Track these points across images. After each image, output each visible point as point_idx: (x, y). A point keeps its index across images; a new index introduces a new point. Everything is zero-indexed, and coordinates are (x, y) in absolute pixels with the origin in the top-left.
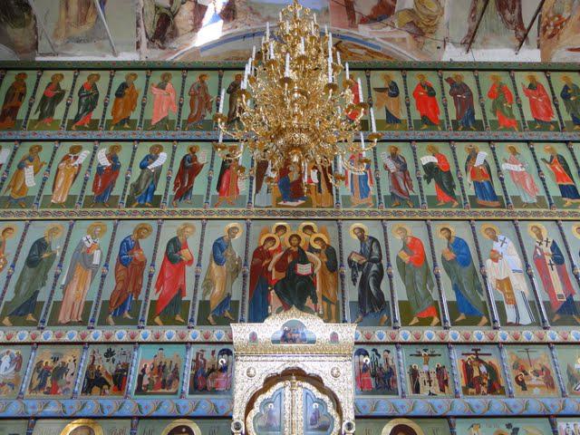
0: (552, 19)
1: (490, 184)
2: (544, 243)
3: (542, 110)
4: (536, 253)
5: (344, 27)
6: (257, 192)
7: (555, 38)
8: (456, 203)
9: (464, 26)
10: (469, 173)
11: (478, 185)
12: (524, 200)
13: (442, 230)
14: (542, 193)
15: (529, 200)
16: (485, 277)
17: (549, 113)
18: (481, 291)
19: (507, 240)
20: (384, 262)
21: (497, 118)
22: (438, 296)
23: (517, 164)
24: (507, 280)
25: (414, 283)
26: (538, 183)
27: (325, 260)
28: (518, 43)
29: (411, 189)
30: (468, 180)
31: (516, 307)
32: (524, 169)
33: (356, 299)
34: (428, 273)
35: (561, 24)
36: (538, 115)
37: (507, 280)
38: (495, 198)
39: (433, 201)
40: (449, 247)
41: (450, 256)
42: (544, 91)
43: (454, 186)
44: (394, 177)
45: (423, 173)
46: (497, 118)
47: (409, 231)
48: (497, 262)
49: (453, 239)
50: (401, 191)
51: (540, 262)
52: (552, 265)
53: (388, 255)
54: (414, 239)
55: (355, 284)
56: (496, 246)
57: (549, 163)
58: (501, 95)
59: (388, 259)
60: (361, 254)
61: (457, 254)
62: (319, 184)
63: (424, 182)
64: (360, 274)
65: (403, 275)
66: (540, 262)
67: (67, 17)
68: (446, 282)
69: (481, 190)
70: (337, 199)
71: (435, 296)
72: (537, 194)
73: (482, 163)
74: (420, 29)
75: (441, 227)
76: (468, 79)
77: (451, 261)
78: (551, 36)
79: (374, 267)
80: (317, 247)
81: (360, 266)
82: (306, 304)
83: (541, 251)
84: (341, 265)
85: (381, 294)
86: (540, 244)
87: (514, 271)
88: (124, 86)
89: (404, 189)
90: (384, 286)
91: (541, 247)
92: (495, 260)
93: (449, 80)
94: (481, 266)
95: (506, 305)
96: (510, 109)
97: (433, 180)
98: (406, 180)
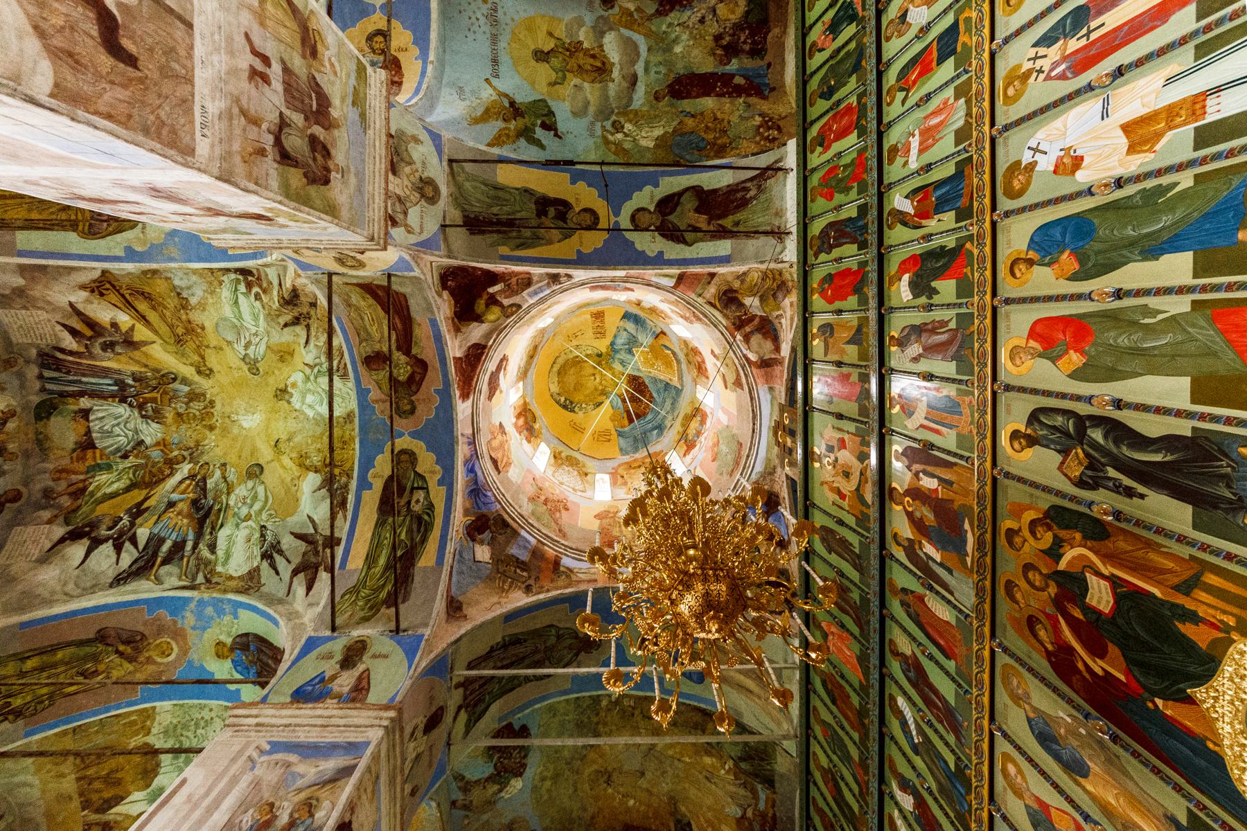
0: (760, 134)
1: (939, 184)
2: (1039, 63)
3: (845, 121)
4: (1062, 77)
5: (782, 372)
6: (952, 593)
7: (781, 123)
8: (968, 245)
9: (764, 244)
10: (924, 222)
11: (940, 208)
12: (961, 123)
13: (1013, 274)
14: (949, 92)
15: (962, 113)
16: (1119, 183)
17: (849, 108)
18: (1161, 190)
19: (1033, 143)
20: (1083, 409)
21: (855, 184)
22: (1174, 298)
23: (909, 143)
24: (1127, 128)
25: (1136, 352)
26: (935, 102)
27: (1078, 536)
28: (780, 173)
29: (947, 323)
30: (932, 224)
31: (1218, 90)
32: (917, 132)
33: (1189, 509)
34: (1111, 317)
35: (767, 122)
36: (850, 127)
37: (1127, 128)
38: (959, 174)
39: (965, 290)
40: (1048, 265)
41: (1067, 260)
42: (826, 124)
43: (942, 248)
44: (930, 350)
45: (923, 300)
46: (855, 184)
47: (1016, 342)
48: (1082, 158)
49: (1031, 255)
50: (949, 343)
51: (1083, 62)
52: (1089, 32)
53: (1063, 396)
54: (1033, 334)
55: (1142, 496)
56: (1045, 164)
57: (908, 91)
58: (834, 183)
59: (1078, 398)
60: (1065, 452)
61: (1061, 247)
62: (940, 480)
63: (936, 299)
64: (1112, 472)
65: (1112, 374)
66: (1083, 62)
67: (759, 698)
68: (1136, 274)
69: (947, 201)
70: (961, 457)
71: (1180, 305)
72: (952, 100)
73: (908, 201)
74: (779, 287)
75: (1010, 278)
76: (816, 228)
77: (1081, 258)
78: (779, 129)
79: (1097, 435)
80: (1047, 539)
81: (1092, 465)
82: (1203, 645)
83: (1055, 65)
84: (1090, 505)
85: (1169, 442)
86: (1040, 71)
87: (1105, 114)
88: (824, 683)
89: (944, 337)
90: (1152, 427)
91: (1046, 69)
92: (1078, 162)
93: (816, 256)
94: (1090, 192)
95: (1209, 119)
96: (845, 166)
97: (933, 284)
98: (933, 331)
